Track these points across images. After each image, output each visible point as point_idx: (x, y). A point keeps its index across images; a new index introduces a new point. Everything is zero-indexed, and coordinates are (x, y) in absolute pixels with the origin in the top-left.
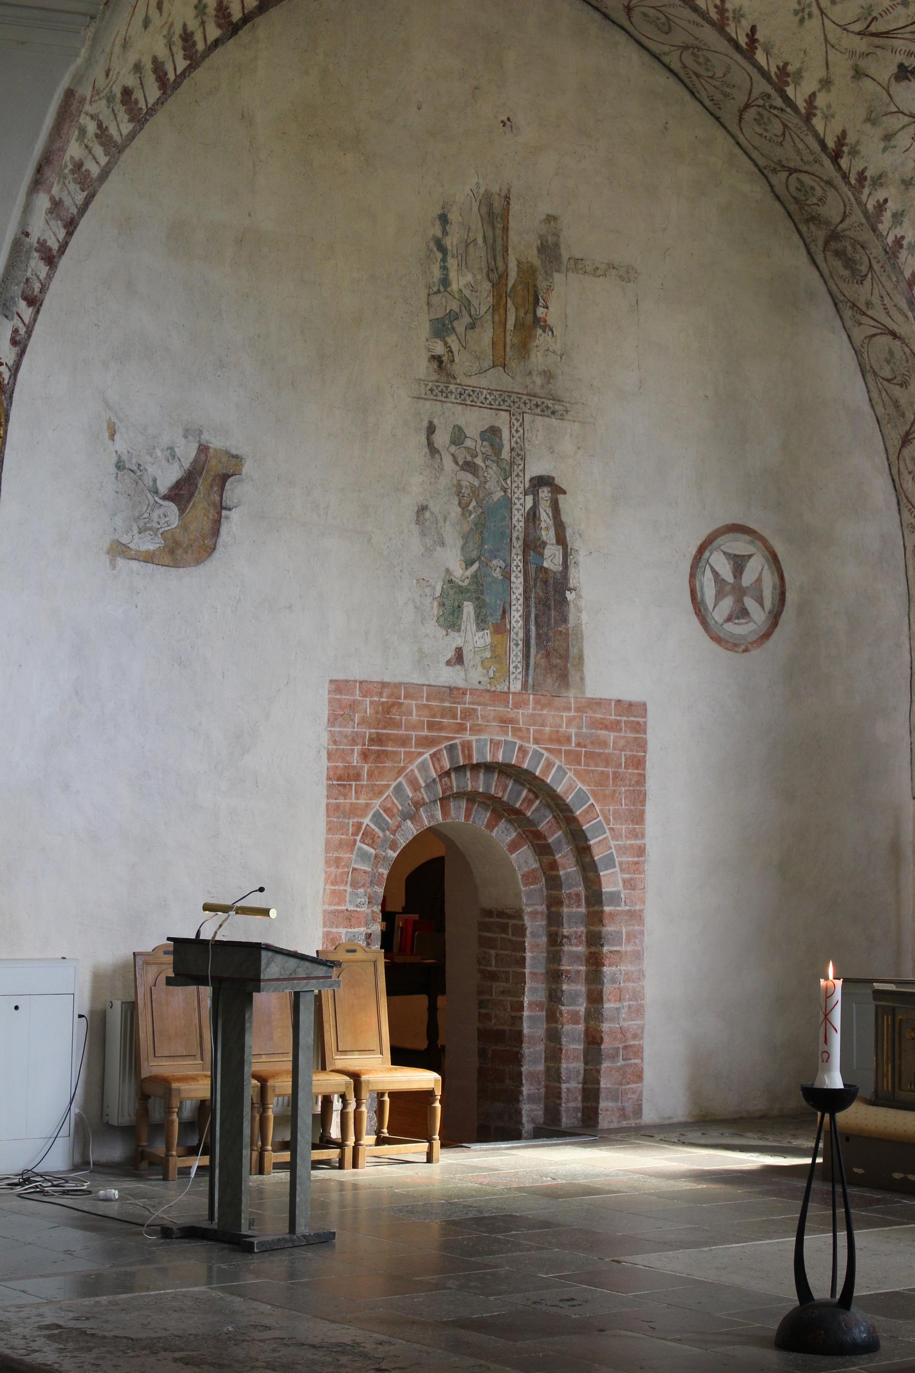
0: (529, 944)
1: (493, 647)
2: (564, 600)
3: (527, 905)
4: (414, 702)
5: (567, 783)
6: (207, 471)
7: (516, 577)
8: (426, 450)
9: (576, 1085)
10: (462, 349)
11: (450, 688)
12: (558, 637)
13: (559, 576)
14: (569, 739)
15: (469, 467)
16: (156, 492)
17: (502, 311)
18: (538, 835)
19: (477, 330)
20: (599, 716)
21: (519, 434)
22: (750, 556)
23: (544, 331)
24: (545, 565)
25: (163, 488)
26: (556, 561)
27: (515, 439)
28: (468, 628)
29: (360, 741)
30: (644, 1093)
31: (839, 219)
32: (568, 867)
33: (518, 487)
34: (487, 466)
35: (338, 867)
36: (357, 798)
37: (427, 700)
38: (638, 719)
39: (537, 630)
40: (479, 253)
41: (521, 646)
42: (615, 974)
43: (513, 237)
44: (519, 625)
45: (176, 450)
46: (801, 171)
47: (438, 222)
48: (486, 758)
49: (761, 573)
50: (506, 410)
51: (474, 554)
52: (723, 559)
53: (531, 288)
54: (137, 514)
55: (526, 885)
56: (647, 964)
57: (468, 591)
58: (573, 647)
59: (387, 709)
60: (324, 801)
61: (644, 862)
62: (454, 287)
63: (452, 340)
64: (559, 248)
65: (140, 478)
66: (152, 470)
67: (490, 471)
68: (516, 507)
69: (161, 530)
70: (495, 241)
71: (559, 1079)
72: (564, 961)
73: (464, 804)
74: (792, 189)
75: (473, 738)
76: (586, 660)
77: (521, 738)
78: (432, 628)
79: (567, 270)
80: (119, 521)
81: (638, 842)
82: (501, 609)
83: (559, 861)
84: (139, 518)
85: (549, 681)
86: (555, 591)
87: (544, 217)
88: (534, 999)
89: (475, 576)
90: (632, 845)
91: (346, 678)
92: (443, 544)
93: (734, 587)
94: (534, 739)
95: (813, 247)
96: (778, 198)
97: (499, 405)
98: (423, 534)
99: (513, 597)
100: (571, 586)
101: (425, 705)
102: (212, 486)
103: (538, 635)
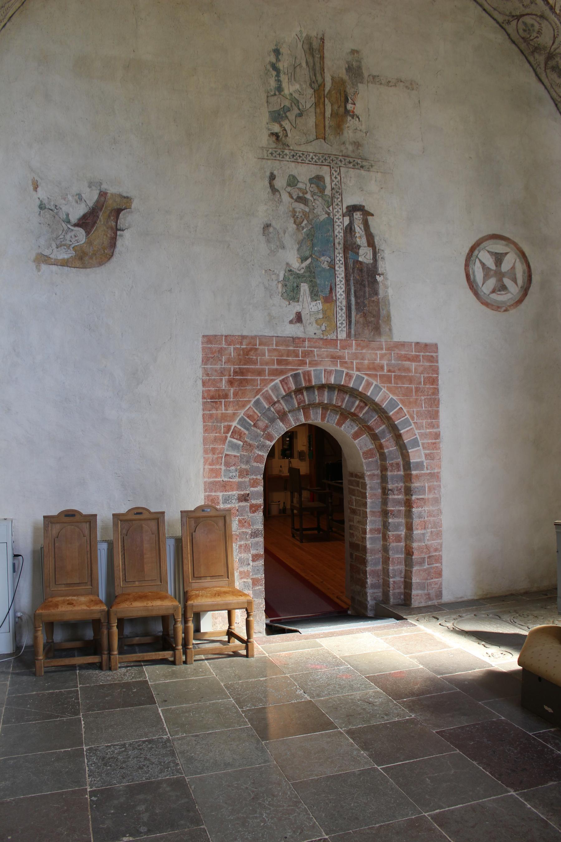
0: (369, 494)
1: (324, 312)
2: (376, 281)
3: (367, 471)
4: (266, 348)
5: (383, 395)
6: (106, 208)
7: (339, 267)
8: (269, 190)
9: (400, 579)
10: (293, 128)
11: (293, 337)
12: (371, 304)
13: (370, 266)
14: (382, 368)
15: (301, 200)
16: (69, 222)
17: (321, 106)
18: (383, 457)
19: (303, 117)
20: (403, 353)
21: (337, 180)
22: (506, 254)
23: (353, 118)
24: (360, 259)
25: (74, 218)
26: (368, 257)
27: (334, 183)
28: (305, 300)
29: (226, 373)
30: (443, 584)
31: (551, 42)
32: (390, 447)
33: (338, 212)
34: (314, 200)
35: (214, 454)
36: (226, 410)
37: (276, 346)
38: (432, 354)
39: (356, 300)
40: (304, 72)
41: (344, 310)
42: (421, 513)
43: (328, 63)
44: (343, 297)
45: (83, 195)
46: (524, 15)
47: (272, 54)
48: (322, 381)
49: (514, 264)
50: (328, 166)
51: (307, 253)
52: (488, 255)
53: (342, 93)
54: (55, 236)
55: (366, 458)
56: (444, 506)
57: (304, 276)
58: (383, 310)
59: (247, 352)
60: (201, 413)
61: (439, 443)
62: (286, 92)
63: (286, 124)
64: (361, 69)
65: (57, 214)
66: (64, 208)
67: (317, 202)
68: (337, 224)
69: (73, 246)
70: (314, 64)
71: (388, 576)
72: (389, 504)
73: (320, 411)
74: (521, 31)
75: (312, 369)
76: (393, 318)
77: (347, 368)
78: (277, 300)
79: (368, 82)
80: (42, 241)
81: (435, 430)
82: (329, 287)
83: (384, 444)
84: (56, 238)
85: (366, 332)
86: (369, 276)
87: (350, 51)
88: (373, 527)
89: (308, 267)
90: (430, 433)
91: (215, 334)
92: (284, 248)
93: (496, 272)
94: (356, 368)
95: (538, 70)
96: (514, 42)
97: (322, 162)
98: (268, 241)
99: (338, 280)
100: (380, 272)
101: (275, 349)
102: (109, 216)
103: (357, 303)
